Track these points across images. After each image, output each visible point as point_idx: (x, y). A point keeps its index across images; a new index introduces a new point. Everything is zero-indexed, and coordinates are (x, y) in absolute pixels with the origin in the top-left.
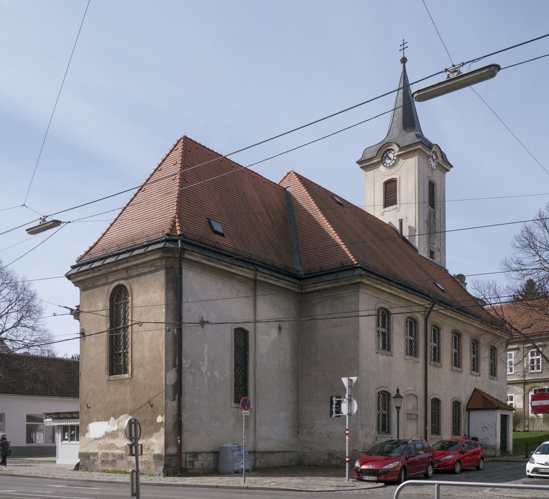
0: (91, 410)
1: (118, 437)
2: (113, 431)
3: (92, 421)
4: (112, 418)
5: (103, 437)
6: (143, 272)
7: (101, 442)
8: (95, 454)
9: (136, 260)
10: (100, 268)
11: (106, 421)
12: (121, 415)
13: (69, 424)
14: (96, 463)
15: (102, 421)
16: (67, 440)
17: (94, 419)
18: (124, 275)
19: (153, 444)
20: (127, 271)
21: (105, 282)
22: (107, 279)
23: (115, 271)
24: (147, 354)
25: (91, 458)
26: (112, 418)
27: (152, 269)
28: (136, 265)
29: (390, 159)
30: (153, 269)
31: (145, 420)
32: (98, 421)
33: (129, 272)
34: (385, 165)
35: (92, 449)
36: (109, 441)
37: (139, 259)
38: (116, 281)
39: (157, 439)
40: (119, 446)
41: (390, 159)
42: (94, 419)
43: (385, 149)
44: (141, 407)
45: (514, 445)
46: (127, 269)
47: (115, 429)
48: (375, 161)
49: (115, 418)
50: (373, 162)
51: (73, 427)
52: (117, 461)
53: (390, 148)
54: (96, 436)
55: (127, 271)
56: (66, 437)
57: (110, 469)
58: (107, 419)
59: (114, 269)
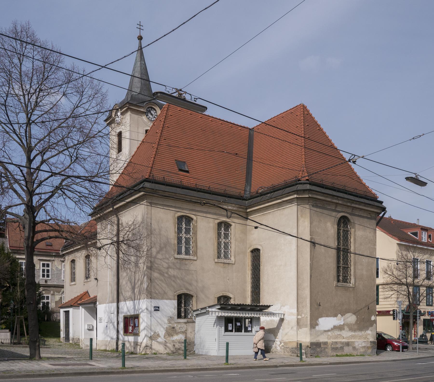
0: (321, 307)
1: (344, 329)
2: (340, 325)
3: (322, 317)
4: (339, 315)
5: (332, 329)
6: (362, 215)
7: (329, 333)
8: (326, 343)
9: (365, 206)
10: (339, 198)
11: (334, 317)
12: (347, 313)
13: (233, 315)
14: (326, 350)
15: (331, 316)
16: (231, 331)
17: (324, 315)
18: (349, 211)
19: (369, 334)
20: (353, 209)
21: (334, 208)
22: (336, 207)
23: (348, 206)
24: (365, 273)
25: (322, 346)
26: (339, 315)
27: (368, 216)
28: (364, 210)
29: (152, 114)
30: (369, 216)
31: (364, 318)
32: (327, 316)
33: (354, 211)
34: (148, 117)
35: (322, 339)
36: (337, 333)
37: (367, 207)
38: (342, 212)
39: (371, 331)
40: (345, 336)
41: (152, 114)
42: (324, 315)
43: (150, 106)
44: (361, 309)
45: (242, 329)
46: (354, 208)
47: (342, 324)
48: (142, 110)
49: (342, 315)
50: (140, 109)
51: (238, 319)
52: (344, 347)
53: (153, 107)
54: (326, 329)
55: (353, 209)
56: (230, 328)
57: (338, 354)
58: (335, 316)
59: (349, 204)
